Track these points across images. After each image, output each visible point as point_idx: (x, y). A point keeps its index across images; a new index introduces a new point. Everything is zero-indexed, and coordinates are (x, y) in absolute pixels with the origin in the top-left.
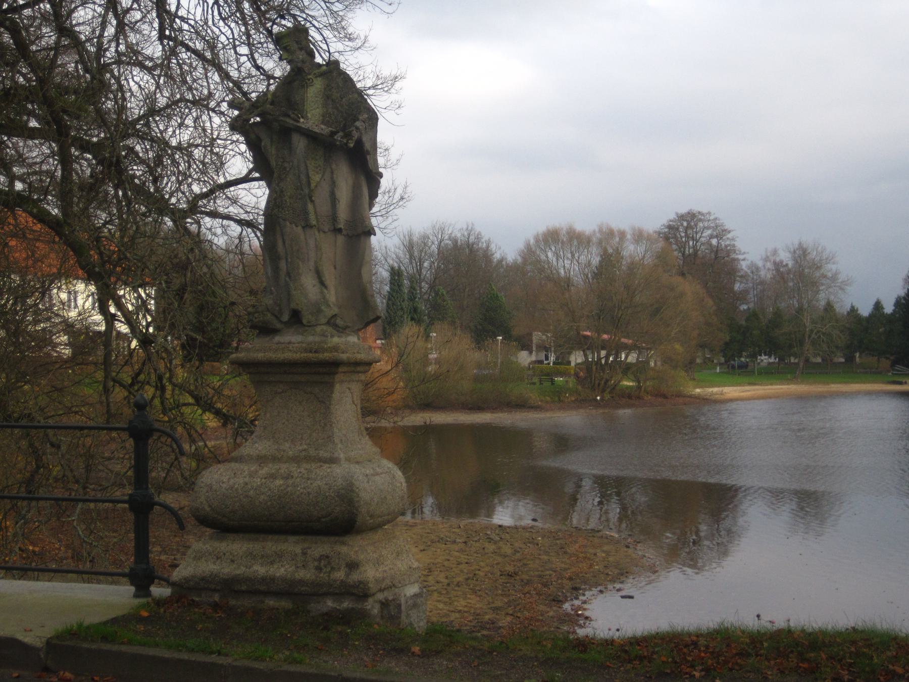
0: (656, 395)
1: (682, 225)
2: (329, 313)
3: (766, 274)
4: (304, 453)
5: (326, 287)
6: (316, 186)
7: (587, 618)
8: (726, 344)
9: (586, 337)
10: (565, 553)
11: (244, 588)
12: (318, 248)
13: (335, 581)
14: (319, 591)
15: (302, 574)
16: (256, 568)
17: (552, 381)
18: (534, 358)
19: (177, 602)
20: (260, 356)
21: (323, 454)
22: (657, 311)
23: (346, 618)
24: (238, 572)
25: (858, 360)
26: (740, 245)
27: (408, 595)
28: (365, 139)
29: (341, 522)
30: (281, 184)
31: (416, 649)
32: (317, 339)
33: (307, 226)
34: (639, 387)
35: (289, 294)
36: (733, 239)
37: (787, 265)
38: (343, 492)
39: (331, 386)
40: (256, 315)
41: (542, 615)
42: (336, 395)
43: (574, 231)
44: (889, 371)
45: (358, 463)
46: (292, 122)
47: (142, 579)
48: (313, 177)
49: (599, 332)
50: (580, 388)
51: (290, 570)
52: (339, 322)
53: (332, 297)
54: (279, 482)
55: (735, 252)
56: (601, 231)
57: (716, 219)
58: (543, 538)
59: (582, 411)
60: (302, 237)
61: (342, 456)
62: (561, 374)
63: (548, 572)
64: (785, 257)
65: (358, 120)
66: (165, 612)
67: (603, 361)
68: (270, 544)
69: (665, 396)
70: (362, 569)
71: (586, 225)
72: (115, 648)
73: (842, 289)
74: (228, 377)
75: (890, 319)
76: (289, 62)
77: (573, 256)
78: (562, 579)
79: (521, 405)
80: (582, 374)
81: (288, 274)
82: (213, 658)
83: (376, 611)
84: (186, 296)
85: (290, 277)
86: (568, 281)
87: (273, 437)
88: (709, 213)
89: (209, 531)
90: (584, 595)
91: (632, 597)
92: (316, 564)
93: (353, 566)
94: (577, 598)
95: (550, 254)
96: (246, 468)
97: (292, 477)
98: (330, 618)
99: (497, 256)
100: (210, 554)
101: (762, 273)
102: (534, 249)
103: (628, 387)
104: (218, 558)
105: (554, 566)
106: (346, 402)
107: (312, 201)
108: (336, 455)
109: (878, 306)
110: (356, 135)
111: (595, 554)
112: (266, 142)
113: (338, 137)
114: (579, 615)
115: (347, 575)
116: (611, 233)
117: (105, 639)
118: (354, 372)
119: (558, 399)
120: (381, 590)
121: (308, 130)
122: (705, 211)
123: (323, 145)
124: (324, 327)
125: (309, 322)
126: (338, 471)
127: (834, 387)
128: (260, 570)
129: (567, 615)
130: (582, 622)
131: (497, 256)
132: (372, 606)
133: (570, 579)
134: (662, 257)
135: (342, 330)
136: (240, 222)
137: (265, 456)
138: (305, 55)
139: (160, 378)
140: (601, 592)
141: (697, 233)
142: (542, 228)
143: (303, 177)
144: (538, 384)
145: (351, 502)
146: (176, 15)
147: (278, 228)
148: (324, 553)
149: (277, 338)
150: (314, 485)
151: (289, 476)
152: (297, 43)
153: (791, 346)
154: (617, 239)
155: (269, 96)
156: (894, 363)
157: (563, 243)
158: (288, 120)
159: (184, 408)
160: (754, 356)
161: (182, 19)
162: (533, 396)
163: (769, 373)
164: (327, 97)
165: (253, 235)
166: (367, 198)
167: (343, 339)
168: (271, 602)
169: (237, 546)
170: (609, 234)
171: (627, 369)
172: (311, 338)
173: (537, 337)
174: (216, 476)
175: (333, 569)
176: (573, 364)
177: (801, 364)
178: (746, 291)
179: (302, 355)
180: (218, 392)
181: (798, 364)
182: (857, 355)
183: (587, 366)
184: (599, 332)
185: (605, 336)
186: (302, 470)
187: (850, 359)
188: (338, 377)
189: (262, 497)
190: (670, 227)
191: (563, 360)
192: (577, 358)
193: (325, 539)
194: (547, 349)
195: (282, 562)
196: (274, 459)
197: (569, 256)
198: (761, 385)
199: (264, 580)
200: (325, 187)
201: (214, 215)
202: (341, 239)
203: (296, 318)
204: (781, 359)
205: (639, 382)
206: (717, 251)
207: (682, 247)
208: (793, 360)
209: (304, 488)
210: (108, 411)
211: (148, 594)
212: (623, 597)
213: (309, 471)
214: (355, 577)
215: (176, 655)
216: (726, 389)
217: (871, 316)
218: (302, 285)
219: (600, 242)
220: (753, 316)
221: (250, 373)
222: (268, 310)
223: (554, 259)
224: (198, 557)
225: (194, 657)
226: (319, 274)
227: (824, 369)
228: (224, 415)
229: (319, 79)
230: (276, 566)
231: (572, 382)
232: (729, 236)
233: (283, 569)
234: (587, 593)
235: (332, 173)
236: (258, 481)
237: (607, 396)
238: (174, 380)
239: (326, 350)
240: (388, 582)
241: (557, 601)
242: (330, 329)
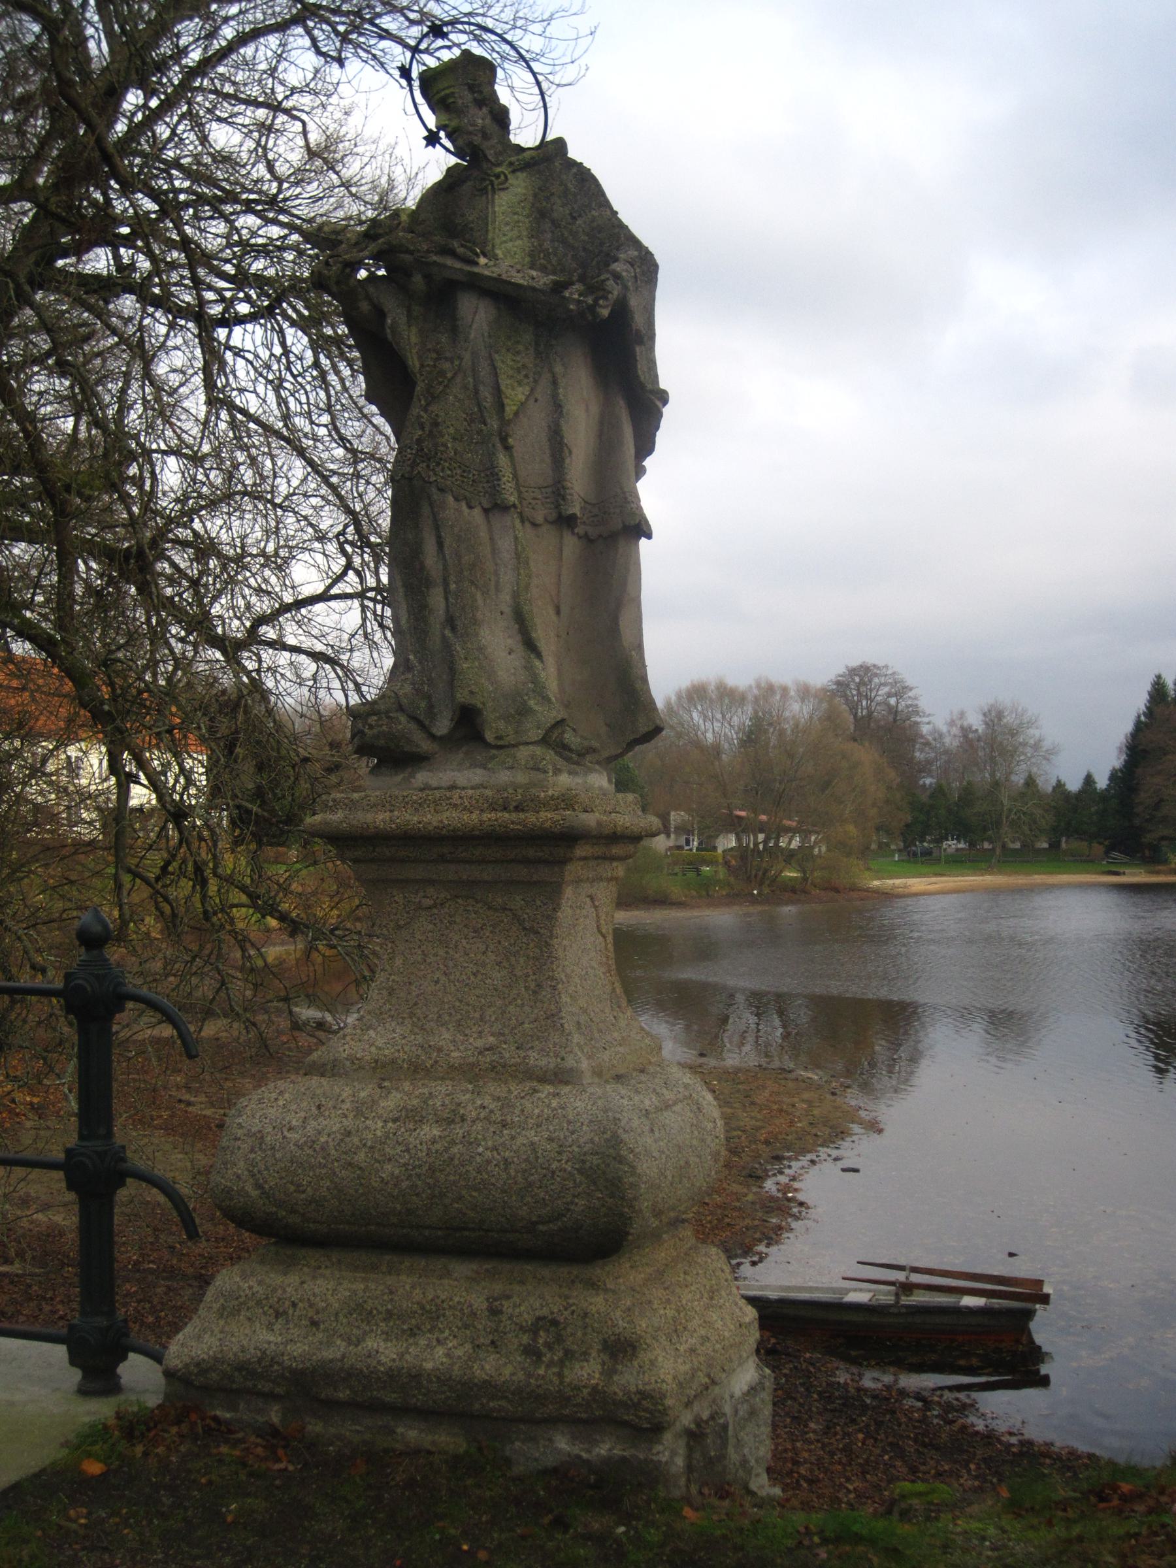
0: (826, 889)
1: (853, 680)
2: (547, 715)
3: (951, 742)
4: (489, 1057)
5: (539, 655)
6: (516, 414)
7: (801, 1204)
8: (907, 826)
9: (739, 817)
10: (753, 1103)
11: (343, 1394)
12: (520, 559)
13: (577, 1388)
14: (538, 1411)
15: (491, 1367)
16: (371, 1344)
17: (698, 871)
19: (178, 1422)
20: (380, 819)
21: (534, 1058)
22: (827, 784)
23: (609, 1488)
24: (328, 1354)
25: (1064, 845)
26: (924, 704)
27: (738, 1393)
28: (634, 302)
30: (434, 408)
32: (521, 778)
34: (805, 879)
35: (452, 670)
36: (916, 698)
37: (977, 730)
38: (596, 1160)
39: (553, 892)
40: (373, 720)
41: (738, 1200)
42: (565, 913)
43: (725, 688)
44: (1103, 859)
45: (618, 1078)
46: (458, 265)
48: (508, 392)
49: (755, 812)
50: (732, 879)
51: (459, 1352)
52: (569, 737)
53: (549, 673)
55: (917, 713)
56: (758, 686)
57: (894, 673)
58: (719, 1081)
59: (736, 908)
60: (483, 534)
61: (585, 1065)
63: (735, 1133)
64: (975, 721)
65: (616, 260)
66: (146, 1454)
67: (761, 847)
69: (837, 891)
70: (644, 1357)
71: (741, 680)
73: (1045, 758)
74: (298, 866)
75: (1104, 796)
77: (724, 717)
78: (755, 1142)
79: (662, 901)
80: (733, 862)
81: (450, 622)
84: (238, 750)
85: (453, 629)
86: (716, 750)
87: (412, 1015)
88: (886, 667)
90: (790, 1167)
91: (856, 1171)
92: (525, 1339)
93: (621, 1349)
94: (781, 1173)
95: (695, 715)
96: (347, 1092)
97: (463, 1119)
100: (259, 1303)
101: (947, 740)
102: (675, 708)
103: (791, 879)
104: (278, 1315)
105: (742, 1124)
106: (585, 923)
107: (508, 448)
108: (570, 1062)
109: (1089, 780)
110: (615, 291)
111: (794, 1106)
112: (396, 316)
113: (573, 293)
114: (789, 1200)
115: (609, 1373)
116: (770, 689)
118: (604, 858)
119: (705, 893)
121: (498, 280)
122: (880, 664)
123: (531, 315)
124: (538, 750)
125: (499, 738)
127: (1038, 879)
128: (383, 1350)
129: (772, 1199)
130: (795, 1210)
132: (670, 1453)
133: (767, 1143)
134: (831, 718)
135: (575, 757)
136: (316, 656)
137: (393, 1061)
138: (488, 121)
139: (199, 869)
140: (813, 1162)
141: (871, 690)
142: (685, 683)
143: (486, 394)
144: (680, 874)
147: (426, 510)
148: (545, 1312)
149: (422, 777)
150: (520, 1140)
152: (471, 88)
153: (985, 829)
154: (778, 697)
155: (404, 218)
156: (1109, 850)
157: (711, 701)
158: (449, 261)
159: (234, 910)
160: (939, 840)
163: (957, 862)
164: (541, 214)
165: (333, 675)
166: (632, 451)
167: (579, 780)
168: (411, 1434)
169: (325, 1286)
170: (769, 690)
171: (790, 856)
172: (504, 777)
174: (272, 1112)
175: (569, 1354)
176: (720, 851)
177: (998, 851)
178: (929, 762)
179: (485, 816)
180: (285, 889)
181: (993, 849)
182: (1064, 839)
183: (742, 853)
184: (755, 812)
185: (764, 818)
186: (487, 1101)
187: (1055, 846)
188: (573, 870)
189: (388, 1167)
190: (838, 683)
191: (707, 846)
192: (728, 842)
193: (546, 1272)
194: (690, 832)
195: (434, 1332)
196: (416, 1070)
197: (719, 716)
198: (949, 876)
199: (392, 1377)
201: (279, 645)
202: (571, 543)
203: (469, 728)
204: (972, 845)
205: (804, 872)
206: (894, 711)
207: (853, 709)
208: (986, 845)
209: (495, 1148)
212: (844, 1170)
213: (505, 1104)
214: (628, 1379)
216: (911, 881)
217: (1081, 792)
218: (481, 649)
219: (756, 699)
220: (939, 792)
221: (356, 861)
222: (401, 708)
223: (701, 722)
224: (228, 1312)
227: (1023, 857)
228: (293, 921)
229: (522, 175)
230: (423, 1342)
231: (722, 873)
232: (910, 694)
233: (440, 1351)
234: (793, 1163)
235: (555, 383)
236: (378, 1127)
237: (766, 891)
238: (220, 871)
239: (544, 804)
241: (756, 1177)
242: (550, 755)
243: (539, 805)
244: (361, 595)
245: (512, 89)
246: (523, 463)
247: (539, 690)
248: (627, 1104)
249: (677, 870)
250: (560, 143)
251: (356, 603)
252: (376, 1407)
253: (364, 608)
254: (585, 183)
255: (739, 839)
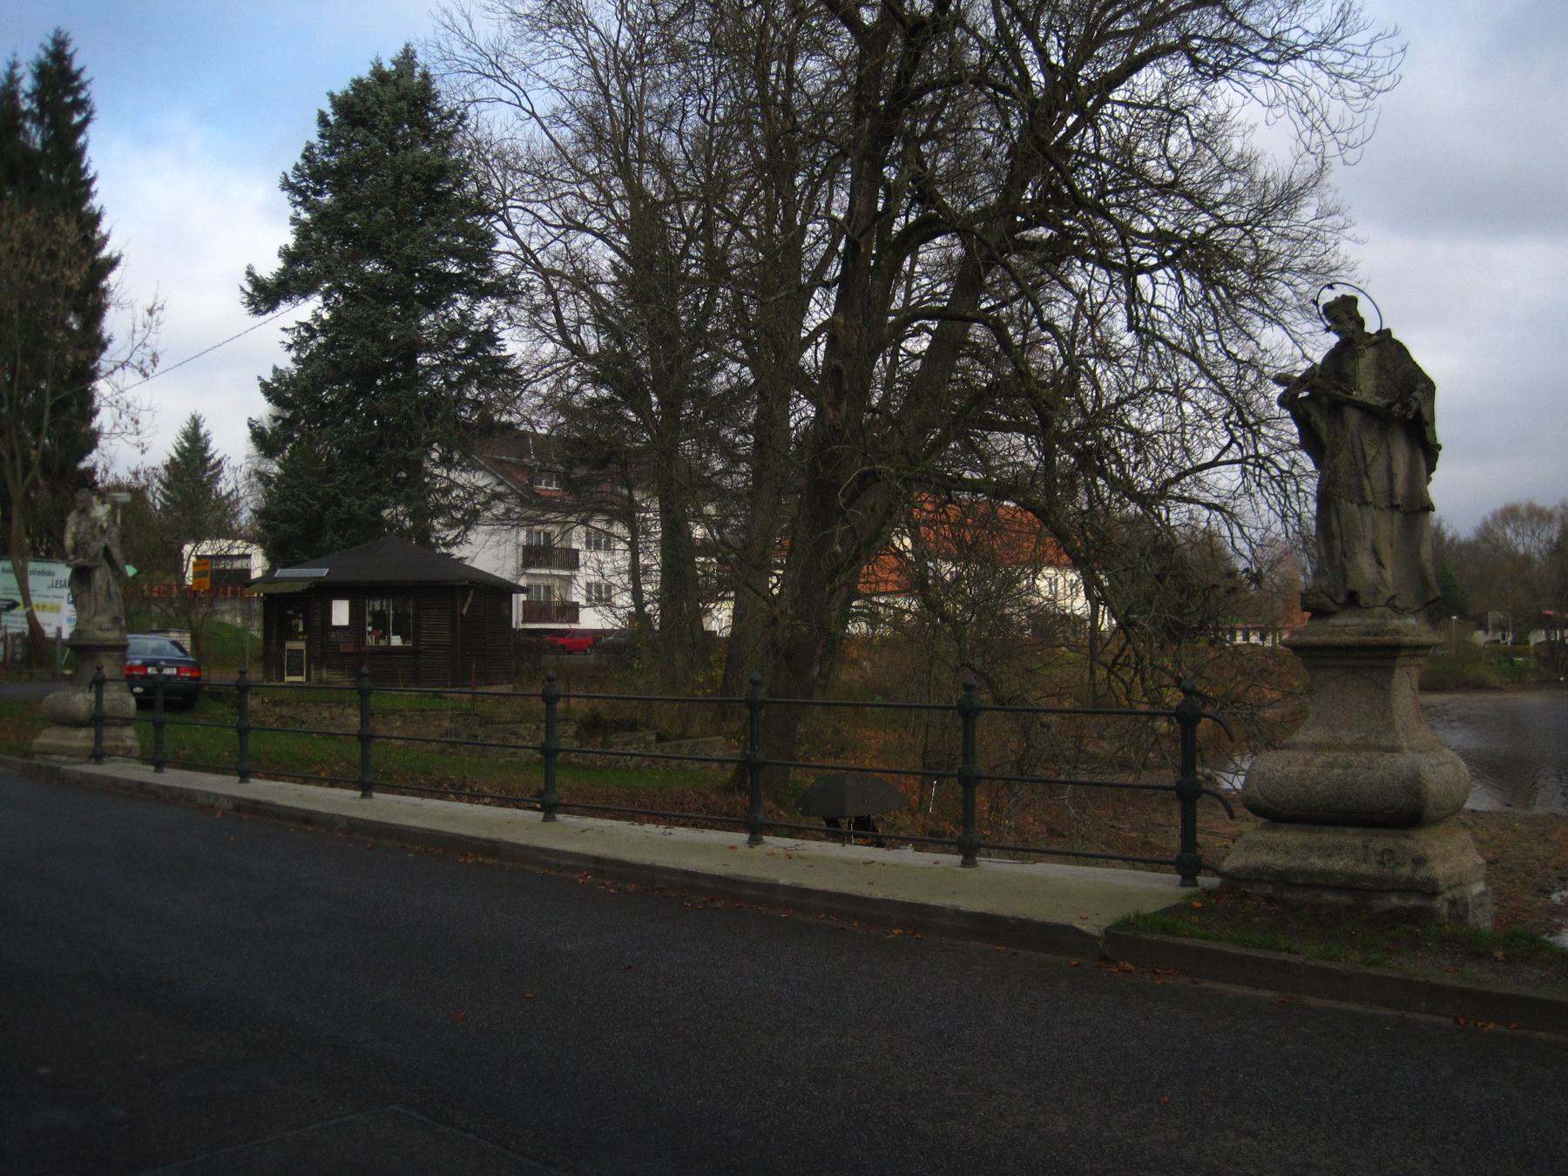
2: (1387, 593)
9: (1547, 616)
12: (1375, 525)
14: (1384, 886)
15: (1363, 868)
17: (1512, 662)
18: (1490, 637)
20: (1314, 639)
21: (1383, 742)
23: (1416, 917)
28: (1424, 409)
29: (1407, 813)
31: (1499, 954)
32: (1376, 621)
33: (1364, 503)
35: (1345, 575)
39: (1391, 671)
42: (1396, 680)
47: (1189, 867)
52: (1397, 603)
54: (1337, 771)
62: (1520, 655)
68: (1326, 836)
72: (1177, 940)
76: (1337, 332)
82: (1283, 956)
83: (1445, 910)
86: (1527, 560)
89: (1261, 820)
93: (1420, 861)
95: (1508, 532)
98: (1395, 916)
99: (1449, 535)
106: (1404, 684)
110: (1414, 406)
112: (1316, 417)
113: (1396, 408)
115: (1414, 871)
117: (1165, 930)
119: (1518, 679)
120: (1449, 888)
126: (1402, 761)
128: (1317, 863)
129: (1556, 906)
131: (1449, 535)
132: (1440, 904)
133: (1556, 868)
135: (1402, 612)
136: (1209, 506)
139: (1140, 659)
142: (1499, 505)
143: (1359, 454)
145: (1417, 794)
146: (1152, 305)
149: (1332, 621)
151: (1348, 765)
157: (1523, 520)
161: (1158, 308)
162: (1492, 678)
164: (1380, 367)
168: (1330, 897)
169: (1292, 837)
172: (1369, 621)
173: (1493, 616)
183: (1550, 645)
188: (1399, 662)
191: (1521, 640)
195: (1342, 854)
196: (1331, 747)
199: (1321, 873)
200: (1381, 462)
202: (1397, 516)
203: (1352, 600)
210: (1094, 693)
211: (1196, 884)
214: (1422, 873)
215: (1244, 951)
219: (1563, 517)
224: (1251, 846)
225: (1262, 954)
226: (1375, 552)
231: (1533, 663)
240: (1456, 880)
243: (1384, 633)
244: (1243, 461)
245: (1364, 308)
246: (1376, 482)
247: (1384, 583)
248: (1425, 763)
249: (1493, 660)
250: (1388, 332)
251: (1237, 467)
252: (1314, 886)
253: (1244, 470)
254: (1401, 349)
255: (1548, 635)
